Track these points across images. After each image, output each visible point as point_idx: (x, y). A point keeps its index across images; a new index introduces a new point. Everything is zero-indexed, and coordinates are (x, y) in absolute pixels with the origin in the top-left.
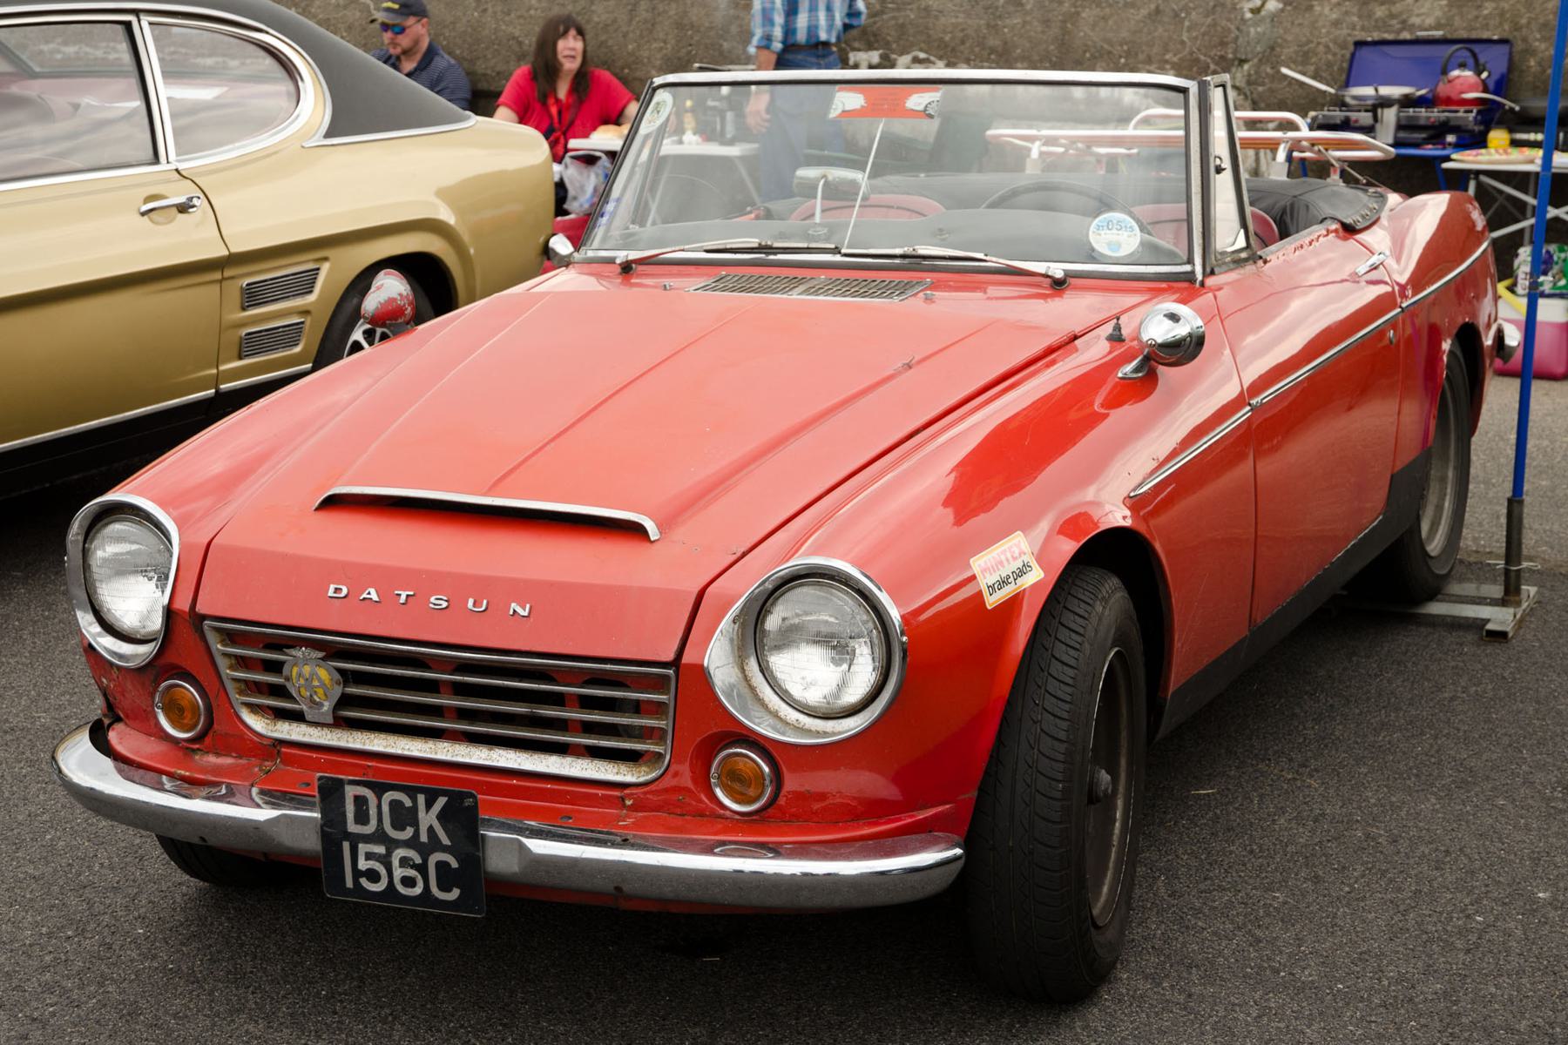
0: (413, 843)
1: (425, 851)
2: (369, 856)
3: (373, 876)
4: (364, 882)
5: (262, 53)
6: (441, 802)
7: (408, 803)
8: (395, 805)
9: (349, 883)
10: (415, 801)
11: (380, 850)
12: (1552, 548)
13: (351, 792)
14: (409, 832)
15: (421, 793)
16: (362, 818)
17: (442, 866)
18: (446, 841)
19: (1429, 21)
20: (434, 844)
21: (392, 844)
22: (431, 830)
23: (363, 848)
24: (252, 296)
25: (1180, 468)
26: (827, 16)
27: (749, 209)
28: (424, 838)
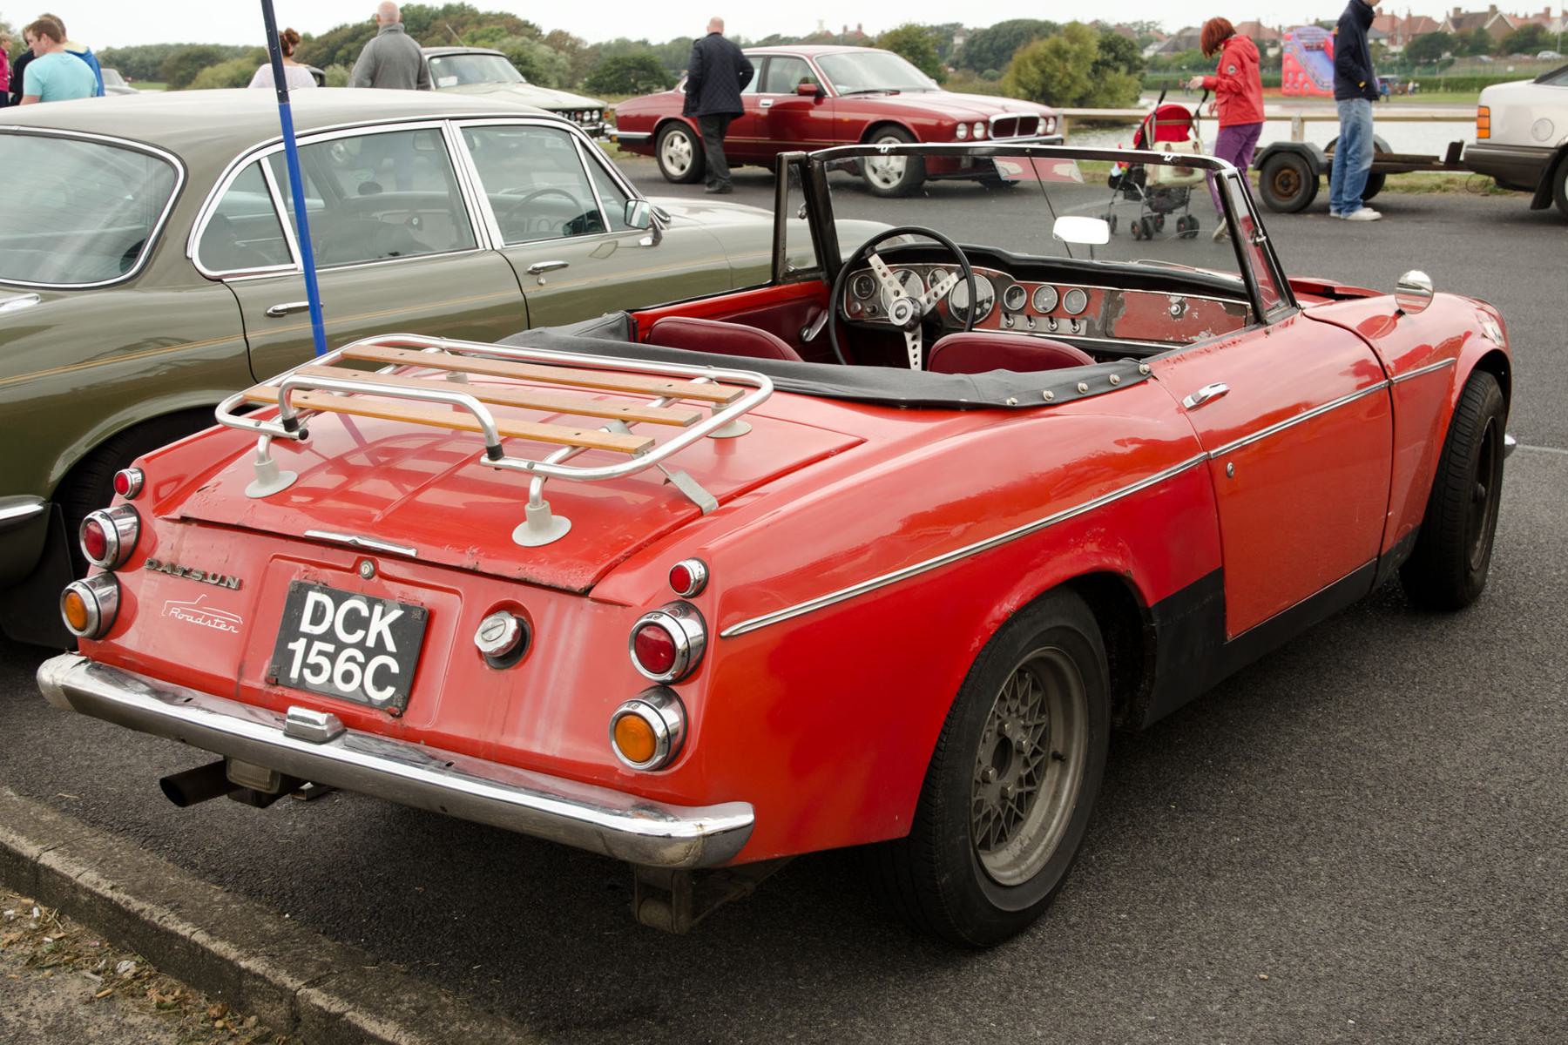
0: (360, 645)
1: (370, 654)
2: (320, 653)
3: (316, 670)
4: (307, 672)
5: (115, 94)
6: (396, 614)
7: (365, 612)
8: (353, 612)
9: (294, 674)
10: (371, 611)
11: (330, 648)
12: (1266, 891)
13: (313, 597)
14: (360, 634)
15: (1200, 167)
16: (317, 618)
17: (383, 668)
18: (391, 646)
19: (1077, 295)
20: (380, 648)
21: (341, 646)
22: (380, 636)
23: (318, 645)
24: (1028, 125)
25: (922, 561)
26: (1270, 81)
27: (1447, 55)
28: (371, 643)
